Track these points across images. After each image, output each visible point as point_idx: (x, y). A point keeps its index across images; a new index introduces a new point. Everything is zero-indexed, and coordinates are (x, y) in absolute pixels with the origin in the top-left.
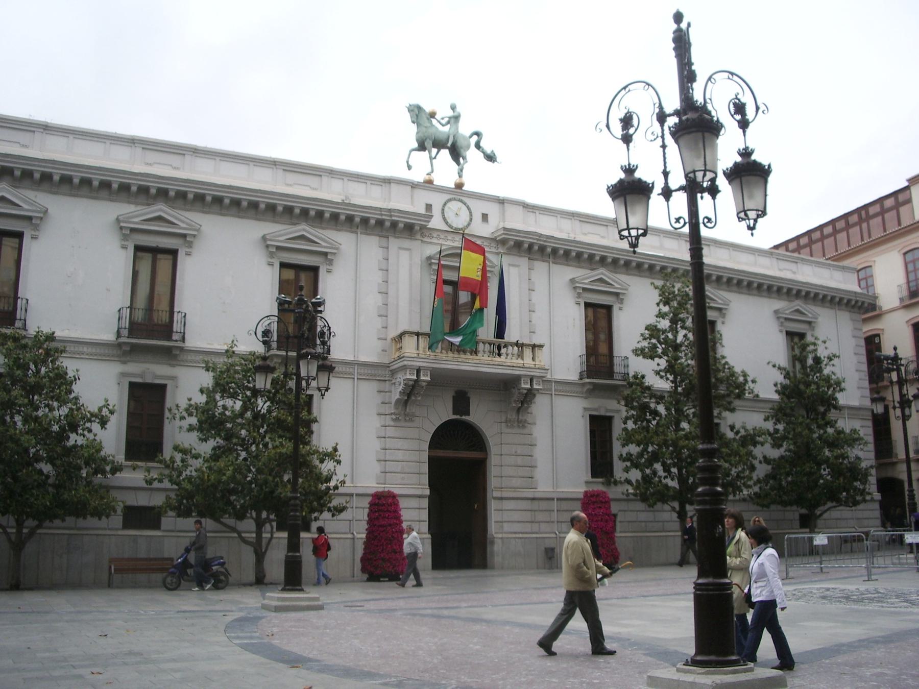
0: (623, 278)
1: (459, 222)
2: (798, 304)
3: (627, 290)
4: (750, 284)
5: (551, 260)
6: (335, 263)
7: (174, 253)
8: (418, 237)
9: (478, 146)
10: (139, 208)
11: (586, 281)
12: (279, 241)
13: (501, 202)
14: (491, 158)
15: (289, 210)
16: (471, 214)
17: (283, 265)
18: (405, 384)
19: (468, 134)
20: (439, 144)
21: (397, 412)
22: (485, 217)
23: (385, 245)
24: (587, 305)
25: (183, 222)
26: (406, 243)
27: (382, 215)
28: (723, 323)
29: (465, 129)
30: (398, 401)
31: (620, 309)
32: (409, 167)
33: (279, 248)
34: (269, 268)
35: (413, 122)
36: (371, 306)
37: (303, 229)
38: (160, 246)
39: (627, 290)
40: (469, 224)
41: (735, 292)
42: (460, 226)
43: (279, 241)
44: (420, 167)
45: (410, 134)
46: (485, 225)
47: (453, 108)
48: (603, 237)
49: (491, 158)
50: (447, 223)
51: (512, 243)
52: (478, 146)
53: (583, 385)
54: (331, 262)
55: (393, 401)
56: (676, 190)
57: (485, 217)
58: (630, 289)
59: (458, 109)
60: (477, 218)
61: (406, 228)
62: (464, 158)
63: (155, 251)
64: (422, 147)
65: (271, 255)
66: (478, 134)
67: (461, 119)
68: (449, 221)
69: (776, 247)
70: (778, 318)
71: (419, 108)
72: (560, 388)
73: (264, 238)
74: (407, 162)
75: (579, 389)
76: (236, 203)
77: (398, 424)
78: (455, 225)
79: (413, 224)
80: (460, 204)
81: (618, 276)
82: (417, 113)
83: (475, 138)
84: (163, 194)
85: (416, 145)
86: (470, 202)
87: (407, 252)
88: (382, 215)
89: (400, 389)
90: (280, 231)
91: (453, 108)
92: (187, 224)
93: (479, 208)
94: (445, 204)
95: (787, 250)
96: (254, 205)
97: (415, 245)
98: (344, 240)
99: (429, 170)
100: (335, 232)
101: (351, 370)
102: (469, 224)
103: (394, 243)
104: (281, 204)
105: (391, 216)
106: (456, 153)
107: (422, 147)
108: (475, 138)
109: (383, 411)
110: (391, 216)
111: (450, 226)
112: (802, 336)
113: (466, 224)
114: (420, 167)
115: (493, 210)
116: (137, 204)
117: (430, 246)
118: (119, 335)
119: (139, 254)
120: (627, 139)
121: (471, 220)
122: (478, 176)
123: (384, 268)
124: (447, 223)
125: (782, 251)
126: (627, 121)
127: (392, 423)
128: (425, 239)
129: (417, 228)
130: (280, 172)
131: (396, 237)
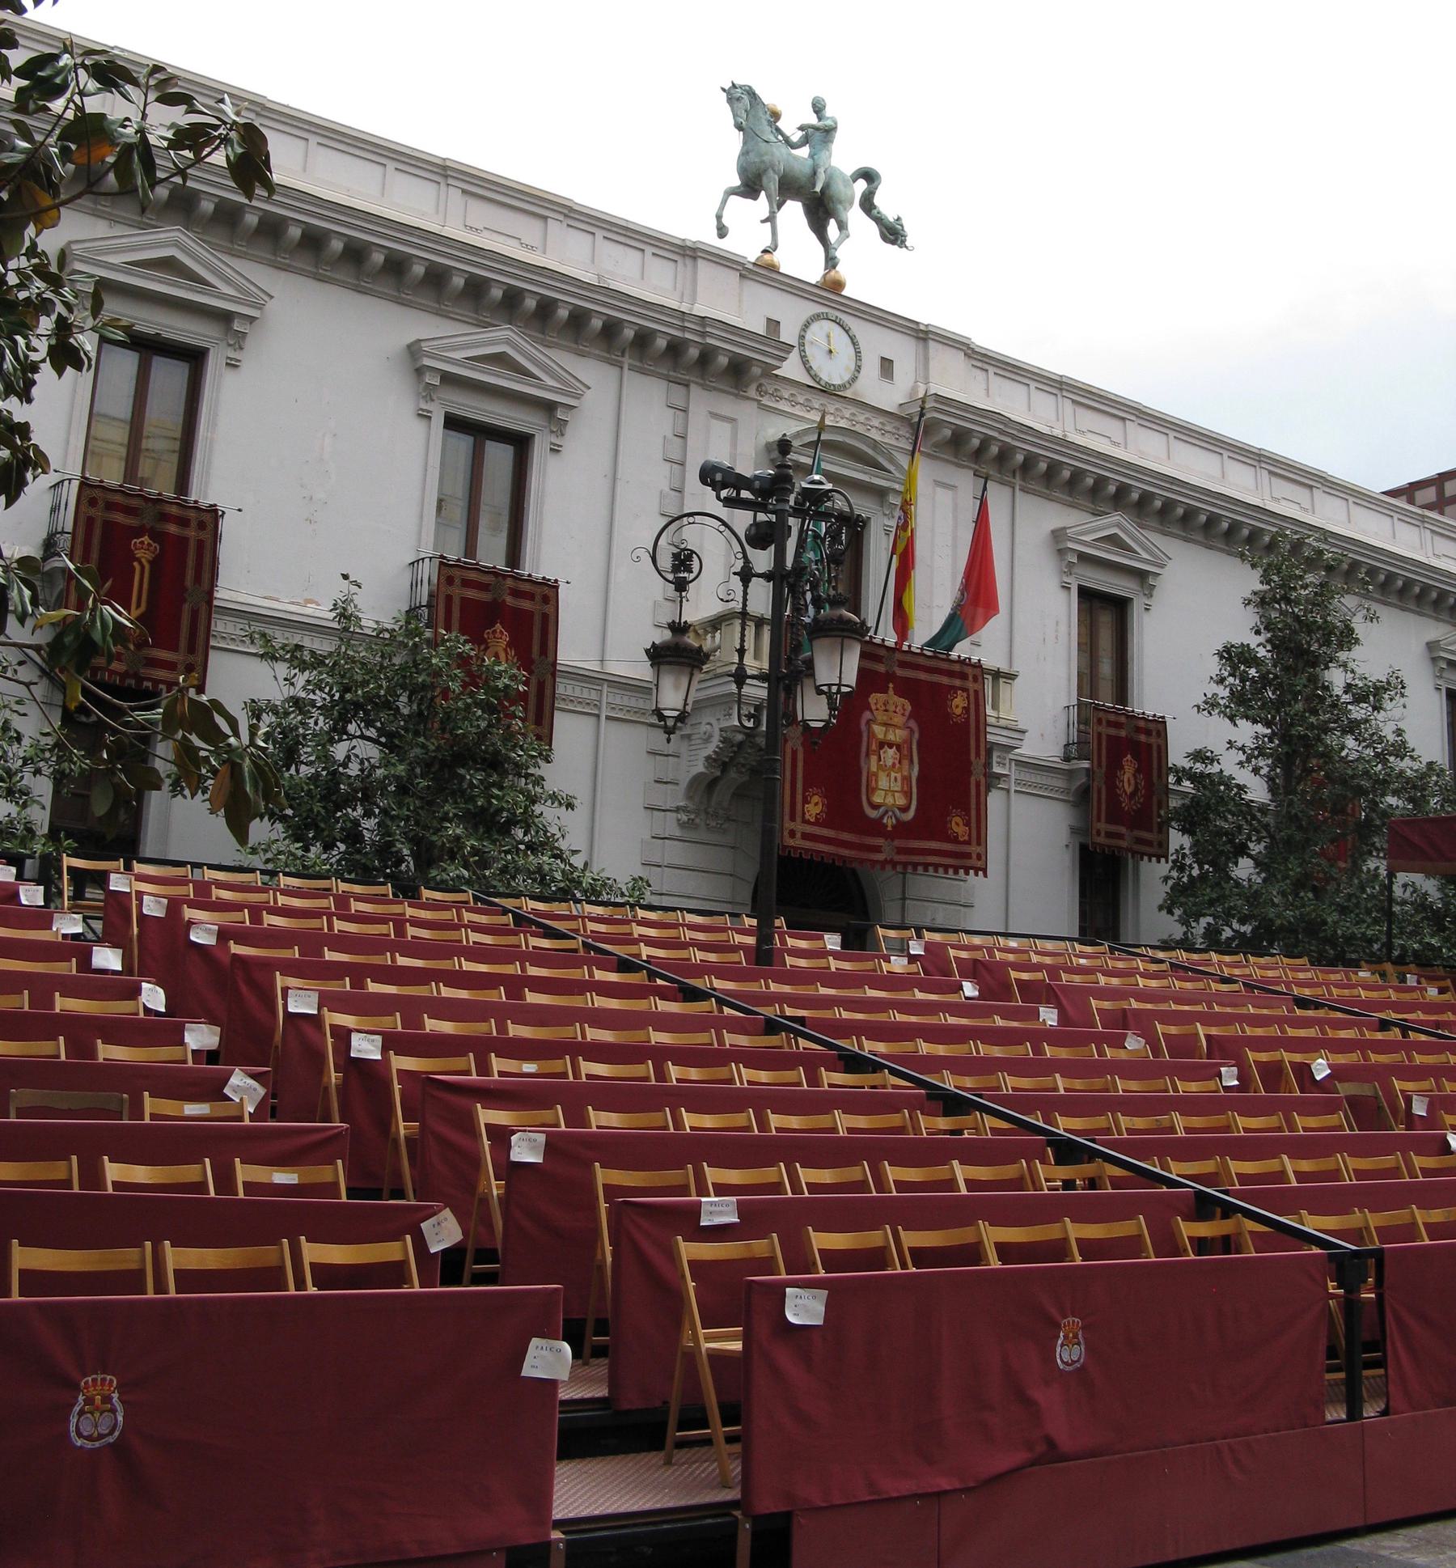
0: (259, 275)
1: (834, 372)
2: (1114, 522)
3: (260, 307)
4: (643, 339)
5: (1018, 481)
6: (249, 343)
7: (194, 357)
8: (752, 392)
9: (868, 205)
10: (119, 230)
11: (458, 355)
12: (1084, 543)
13: (922, 335)
14: (893, 234)
15: (476, 289)
16: (858, 353)
17: (454, 423)
18: (725, 740)
19: (849, 170)
20: (790, 187)
21: (691, 806)
22: (887, 366)
23: (681, 403)
24: (1085, 594)
25: (228, 281)
26: (727, 405)
27: (684, 329)
28: (555, 450)
29: (843, 158)
30: (696, 780)
31: (555, 450)
32: (722, 232)
33: (448, 379)
34: (419, 426)
35: (739, 127)
36: (621, 534)
37: (503, 338)
38: (165, 335)
39: (578, 397)
40: (854, 379)
41: (1222, 550)
42: (837, 381)
43: (1084, 543)
44: (747, 229)
45: (725, 150)
46: (885, 384)
47: (818, 108)
48: (1306, 510)
49: (893, 234)
50: (809, 369)
51: (948, 433)
52: (868, 205)
53: (1070, 774)
54: (560, 427)
55: (685, 779)
56: (753, 677)
57: (887, 366)
58: (271, 305)
59: (829, 112)
60: (871, 367)
61: (701, 361)
62: (842, 226)
63: (147, 346)
64: (750, 187)
65: (429, 392)
66: (869, 176)
67: (839, 137)
68: (814, 364)
69: (1391, 493)
70: (1434, 660)
71: (752, 94)
72: (1025, 776)
73: (414, 350)
74: (719, 217)
75: (1059, 782)
76: (355, 254)
77: (688, 835)
78: (825, 377)
79: (285, 219)
80: (836, 331)
81: (554, 354)
82: (746, 105)
83: (861, 186)
84: (1120, 498)
85: (736, 182)
86: (864, 331)
87: (727, 426)
88: (684, 329)
89: (710, 749)
90: (459, 341)
91: (818, 108)
92: (238, 288)
93: (877, 342)
94: (806, 326)
95: (1411, 501)
96: (396, 266)
97: (745, 411)
98: (594, 383)
99: (767, 242)
100: (572, 357)
101: (594, 695)
102: (854, 379)
103: (701, 401)
104: (462, 270)
105: (703, 334)
106: (821, 210)
107: (750, 187)
108: (861, 186)
109: (660, 803)
110: (703, 334)
111: (814, 377)
112: (1120, 606)
113: (847, 377)
114: (747, 229)
115: (902, 351)
116: (113, 220)
117: (774, 418)
118: (50, 546)
119: (106, 346)
120: (681, 586)
121: (858, 369)
122: (868, 269)
123: (676, 457)
124: (809, 369)
125: (1401, 503)
126: (684, 560)
127: (677, 833)
128: (765, 401)
129: (756, 370)
130: (455, 195)
131: (705, 387)
